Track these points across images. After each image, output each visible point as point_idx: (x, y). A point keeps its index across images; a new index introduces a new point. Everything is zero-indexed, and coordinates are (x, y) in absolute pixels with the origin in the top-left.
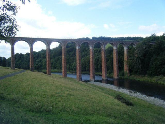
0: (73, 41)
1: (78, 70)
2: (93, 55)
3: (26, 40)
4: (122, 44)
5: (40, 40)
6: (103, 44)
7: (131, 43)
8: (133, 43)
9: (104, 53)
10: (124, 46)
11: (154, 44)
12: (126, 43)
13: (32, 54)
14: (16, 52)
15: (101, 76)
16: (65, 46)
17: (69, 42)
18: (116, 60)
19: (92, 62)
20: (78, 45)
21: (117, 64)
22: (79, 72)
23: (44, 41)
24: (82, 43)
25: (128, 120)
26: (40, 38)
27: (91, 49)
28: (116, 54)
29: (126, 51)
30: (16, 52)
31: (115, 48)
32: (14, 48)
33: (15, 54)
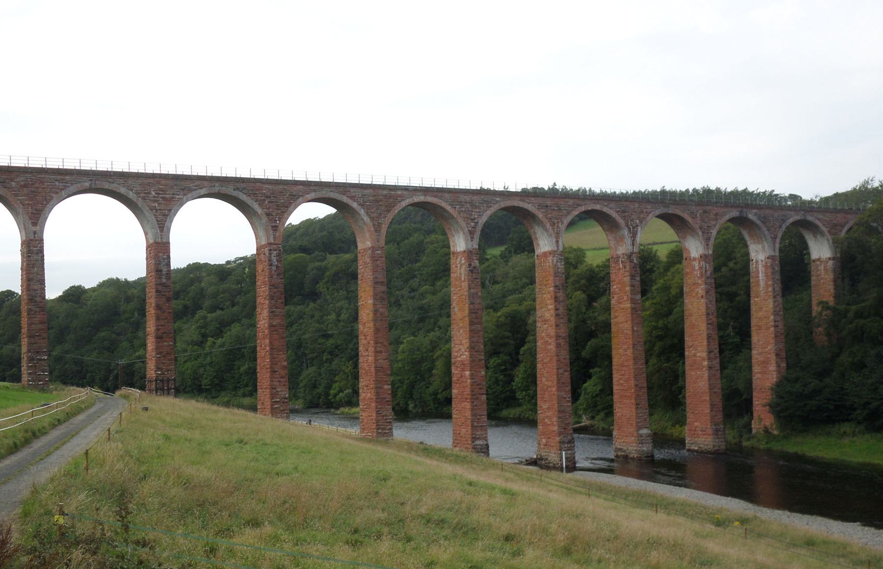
0: (430, 199)
1: (468, 390)
2: (561, 295)
3: (123, 190)
4: (741, 221)
5: (216, 190)
6: (622, 222)
7: (797, 218)
8: (810, 218)
9: (627, 279)
10: (751, 236)
11: (542, 191)
12: (765, 220)
13: (163, 285)
14: (179, 259)
15: (608, 435)
16: (377, 228)
17: (404, 204)
18: (703, 327)
19: (552, 341)
20: (463, 224)
21: (710, 352)
22: (468, 405)
23: (243, 197)
24: (489, 212)
25: (727, 523)
26: (157, 171)
27: (545, 254)
28: (701, 290)
29: (761, 269)
30: (179, 259)
31: (695, 248)
32: (41, 241)
33: (53, 291)
